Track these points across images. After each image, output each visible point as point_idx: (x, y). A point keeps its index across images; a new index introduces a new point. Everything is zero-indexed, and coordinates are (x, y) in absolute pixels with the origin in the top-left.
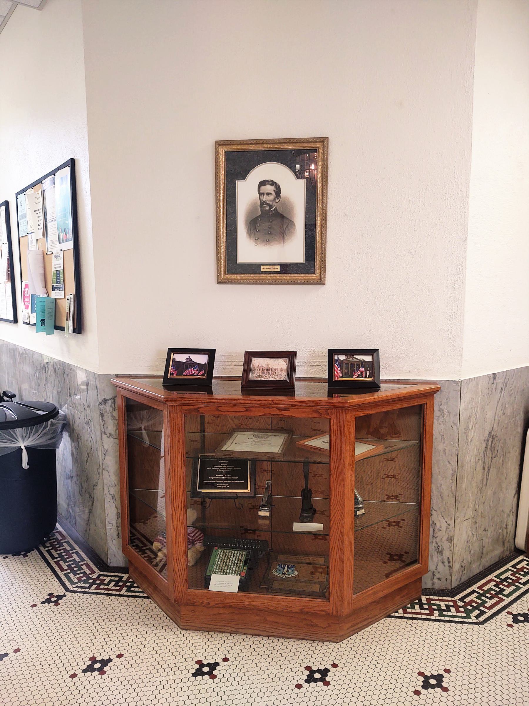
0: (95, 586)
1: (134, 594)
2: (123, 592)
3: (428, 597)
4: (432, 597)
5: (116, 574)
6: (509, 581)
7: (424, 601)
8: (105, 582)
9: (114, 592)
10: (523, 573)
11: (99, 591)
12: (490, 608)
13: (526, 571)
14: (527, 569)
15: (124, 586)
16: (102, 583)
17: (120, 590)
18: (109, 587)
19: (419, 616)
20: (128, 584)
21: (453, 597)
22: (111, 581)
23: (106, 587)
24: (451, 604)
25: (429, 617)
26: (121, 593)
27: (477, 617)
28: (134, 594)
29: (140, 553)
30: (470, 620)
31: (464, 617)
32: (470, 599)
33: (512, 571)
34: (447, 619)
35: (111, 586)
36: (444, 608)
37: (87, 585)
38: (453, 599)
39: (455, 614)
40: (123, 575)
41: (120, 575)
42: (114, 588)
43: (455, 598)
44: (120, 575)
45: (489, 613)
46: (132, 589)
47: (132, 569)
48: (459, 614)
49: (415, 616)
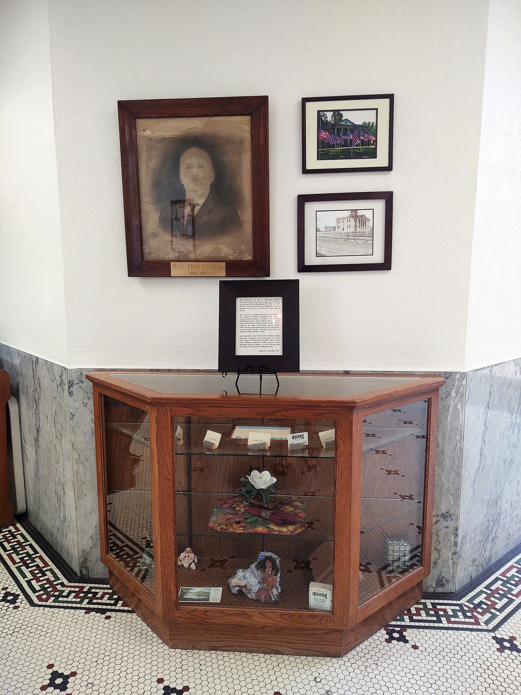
0: (87, 601)
1: (61, 604)
2: (85, 604)
3: (432, 601)
4: (437, 601)
5: (77, 584)
6: (484, 606)
7: (430, 606)
8: (73, 594)
9: (74, 605)
10: (498, 596)
11: (57, 604)
12: (501, 610)
13: (517, 579)
14: (518, 577)
15: (85, 597)
16: (60, 596)
17: (81, 602)
18: (103, 601)
19: (427, 624)
20: (82, 595)
21: (459, 599)
22: (104, 594)
23: (65, 599)
24: (458, 608)
25: (436, 625)
26: (117, 608)
27: (487, 623)
28: (61, 604)
29: (117, 560)
30: (479, 627)
31: (472, 624)
32: (479, 601)
33: (517, 568)
34: (456, 626)
35: (71, 598)
36: (450, 613)
37: (78, 600)
38: (459, 602)
39: (425, 618)
40: (84, 585)
41: (81, 585)
42: (74, 600)
43: (461, 601)
44: (81, 585)
45: (501, 616)
46: (61, 599)
47: (114, 576)
48: (429, 618)
49: (422, 624)
